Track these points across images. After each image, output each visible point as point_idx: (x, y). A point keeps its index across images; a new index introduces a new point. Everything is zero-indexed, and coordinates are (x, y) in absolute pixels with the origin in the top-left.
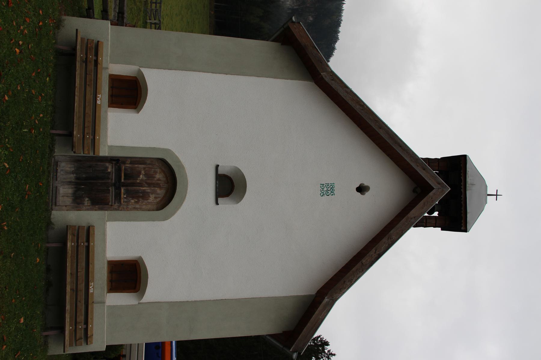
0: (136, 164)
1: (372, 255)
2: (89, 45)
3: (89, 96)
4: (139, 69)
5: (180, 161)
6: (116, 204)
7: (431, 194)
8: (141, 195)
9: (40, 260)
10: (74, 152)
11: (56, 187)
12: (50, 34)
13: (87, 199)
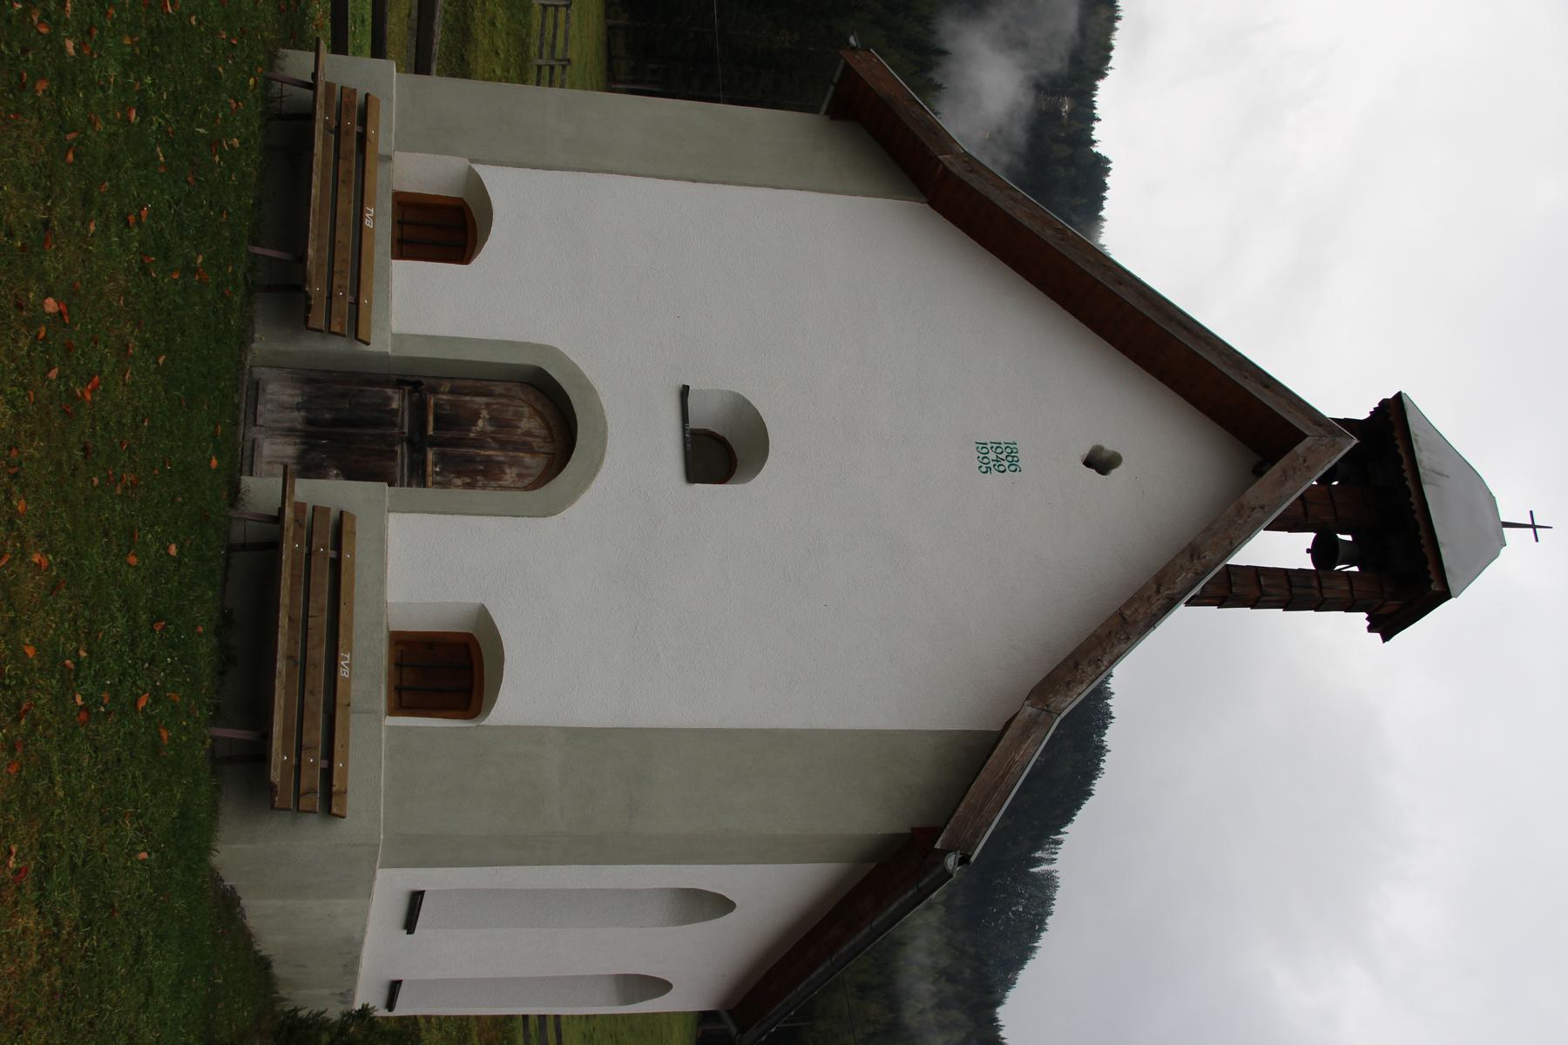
0: (467, 395)
1: (1149, 597)
3: (346, 206)
4: (471, 172)
5: (582, 375)
7: (1300, 448)
8: (482, 467)
11: (254, 441)
13: (335, 472)
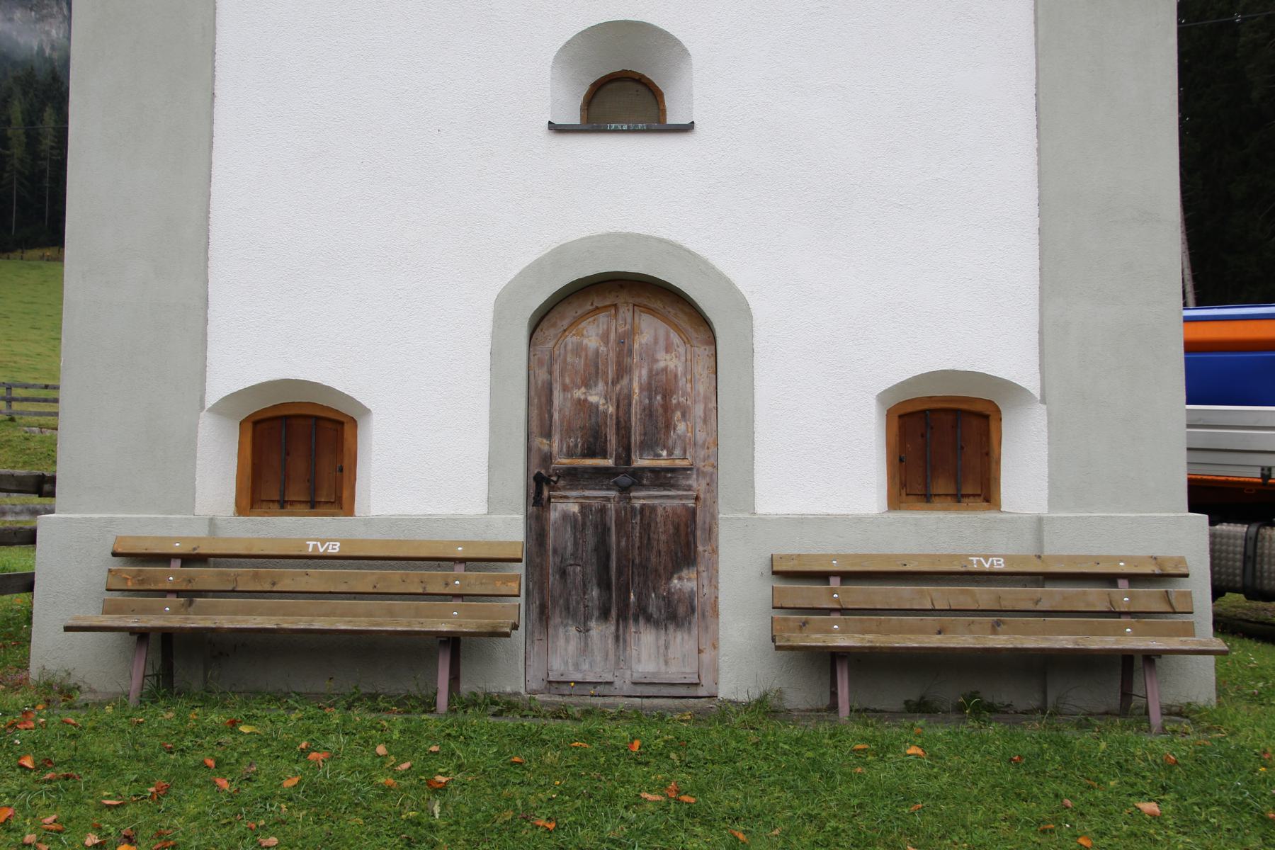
0: (551, 417)
2: (130, 583)
3: (315, 579)
4: (210, 410)
5: (539, 263)
6: (692, 482)
8: (659, 398)
9: (912, 743)
10: (515, 627)
12: (75, 725)
